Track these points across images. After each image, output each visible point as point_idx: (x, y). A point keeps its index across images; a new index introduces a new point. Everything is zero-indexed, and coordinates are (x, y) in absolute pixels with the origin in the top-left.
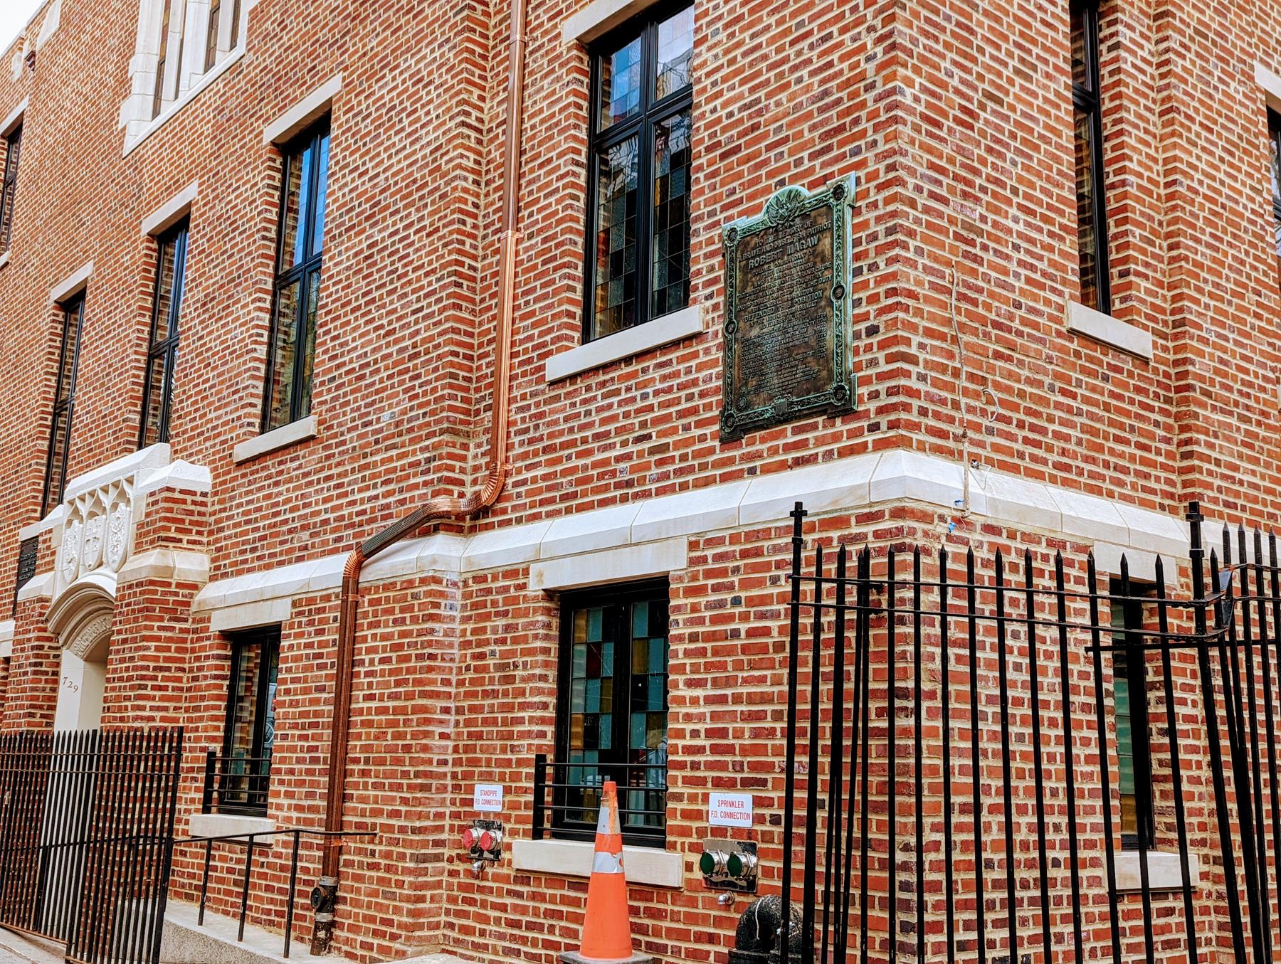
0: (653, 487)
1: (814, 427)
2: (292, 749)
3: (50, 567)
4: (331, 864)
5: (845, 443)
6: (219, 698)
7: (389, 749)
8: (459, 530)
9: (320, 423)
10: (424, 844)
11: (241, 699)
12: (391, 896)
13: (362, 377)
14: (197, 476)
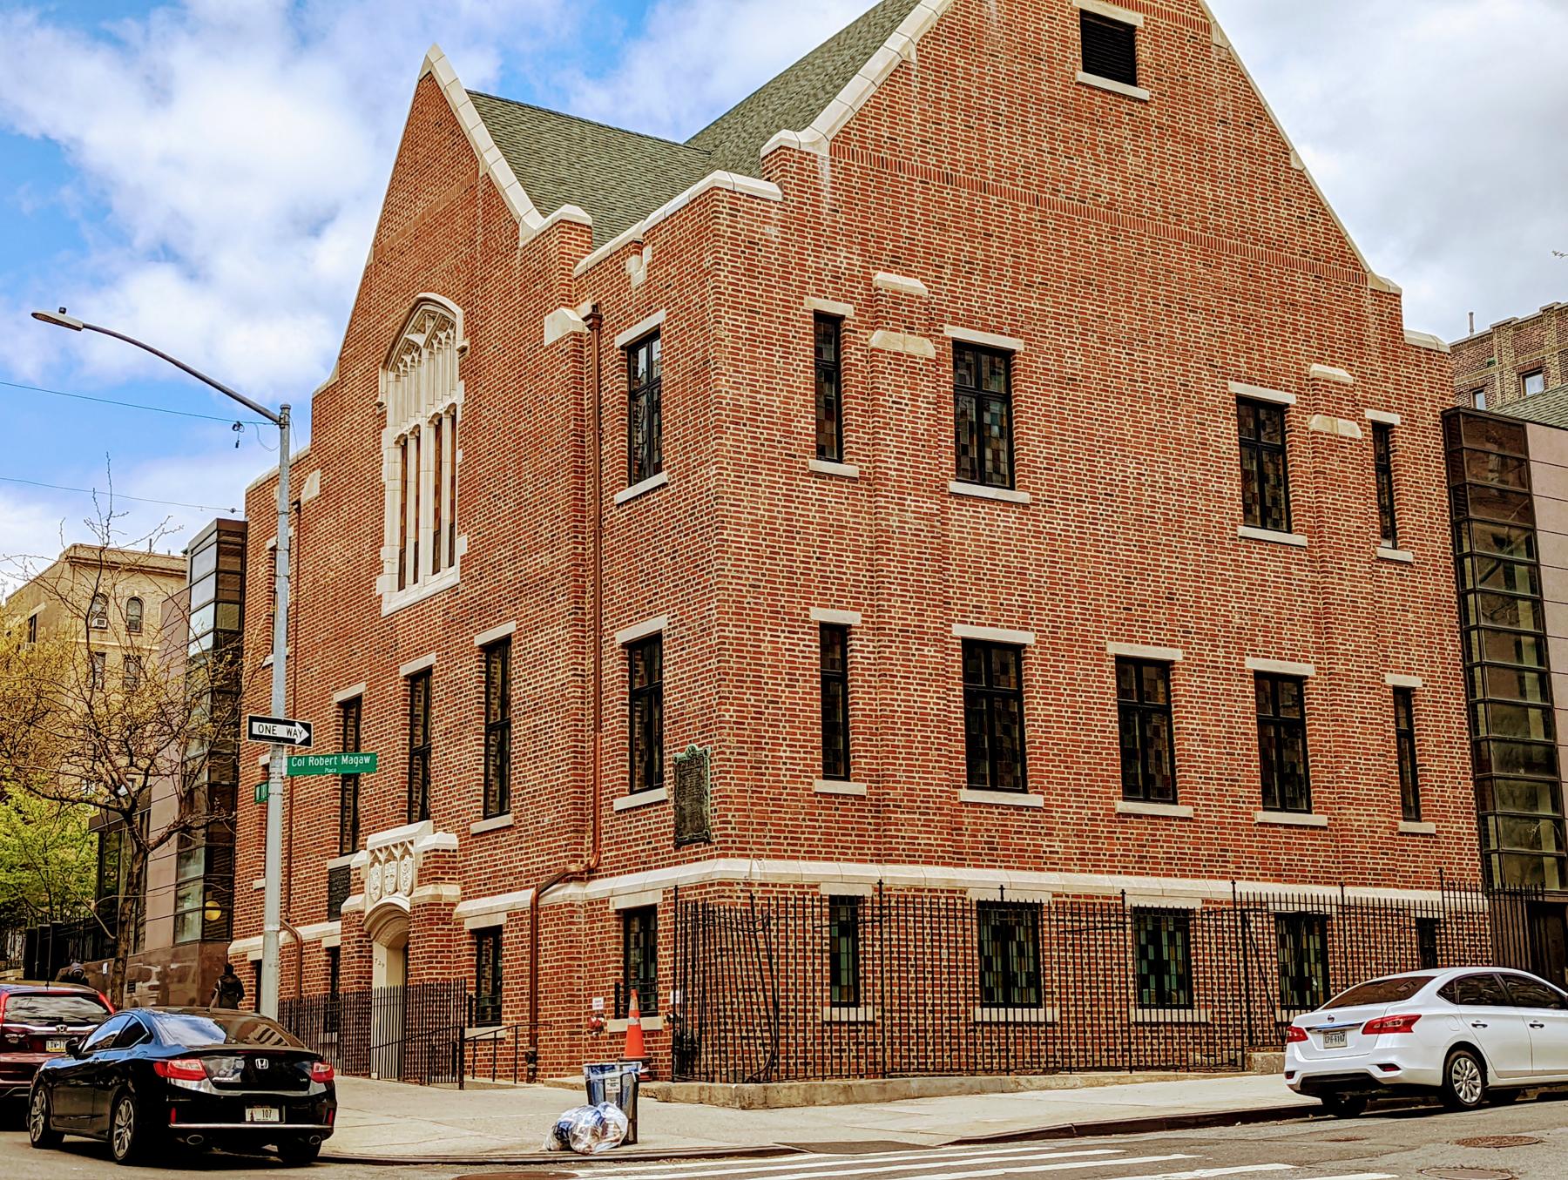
2: (512, 990)
3: (361, 891)
4: (533, 1040)
6: (472, 966)
7: (556, 985)
8: (582, 880)
9: (516, 818)
10: (572, 1027)
11: (484, 966)
12: (560, 1052)
13: (534, 797)
14: (450, 840)
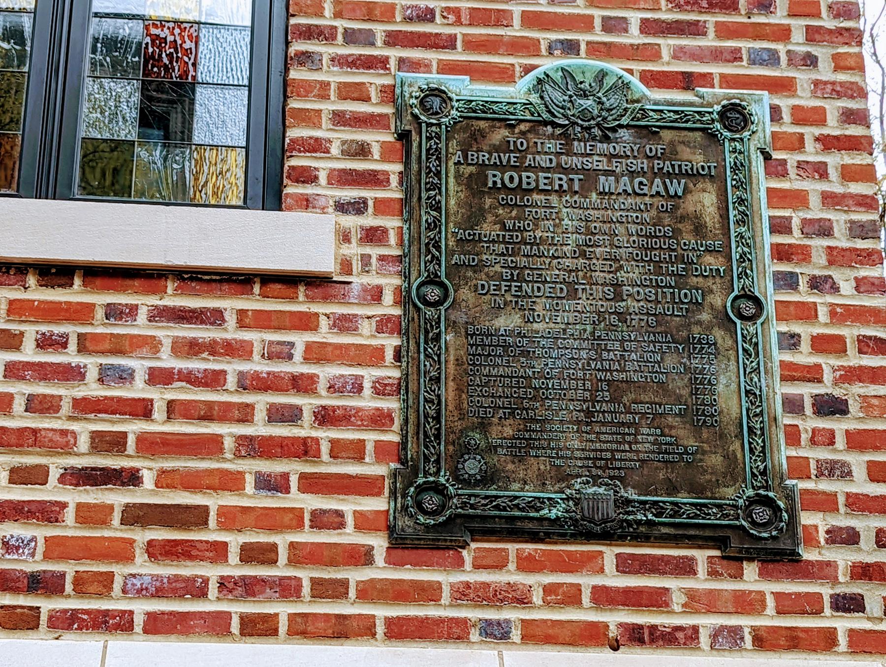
0: (140, 608)
1: (686, 568)
5: (770, 619)
